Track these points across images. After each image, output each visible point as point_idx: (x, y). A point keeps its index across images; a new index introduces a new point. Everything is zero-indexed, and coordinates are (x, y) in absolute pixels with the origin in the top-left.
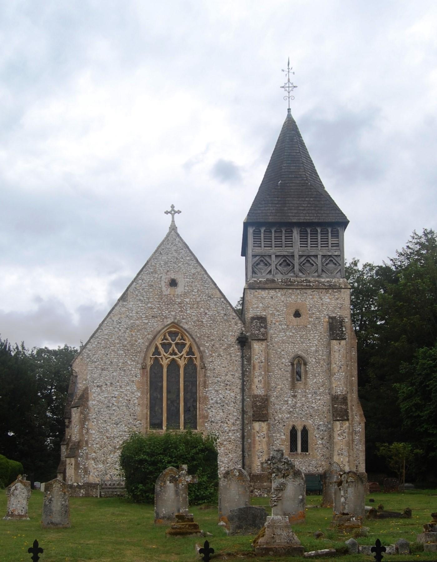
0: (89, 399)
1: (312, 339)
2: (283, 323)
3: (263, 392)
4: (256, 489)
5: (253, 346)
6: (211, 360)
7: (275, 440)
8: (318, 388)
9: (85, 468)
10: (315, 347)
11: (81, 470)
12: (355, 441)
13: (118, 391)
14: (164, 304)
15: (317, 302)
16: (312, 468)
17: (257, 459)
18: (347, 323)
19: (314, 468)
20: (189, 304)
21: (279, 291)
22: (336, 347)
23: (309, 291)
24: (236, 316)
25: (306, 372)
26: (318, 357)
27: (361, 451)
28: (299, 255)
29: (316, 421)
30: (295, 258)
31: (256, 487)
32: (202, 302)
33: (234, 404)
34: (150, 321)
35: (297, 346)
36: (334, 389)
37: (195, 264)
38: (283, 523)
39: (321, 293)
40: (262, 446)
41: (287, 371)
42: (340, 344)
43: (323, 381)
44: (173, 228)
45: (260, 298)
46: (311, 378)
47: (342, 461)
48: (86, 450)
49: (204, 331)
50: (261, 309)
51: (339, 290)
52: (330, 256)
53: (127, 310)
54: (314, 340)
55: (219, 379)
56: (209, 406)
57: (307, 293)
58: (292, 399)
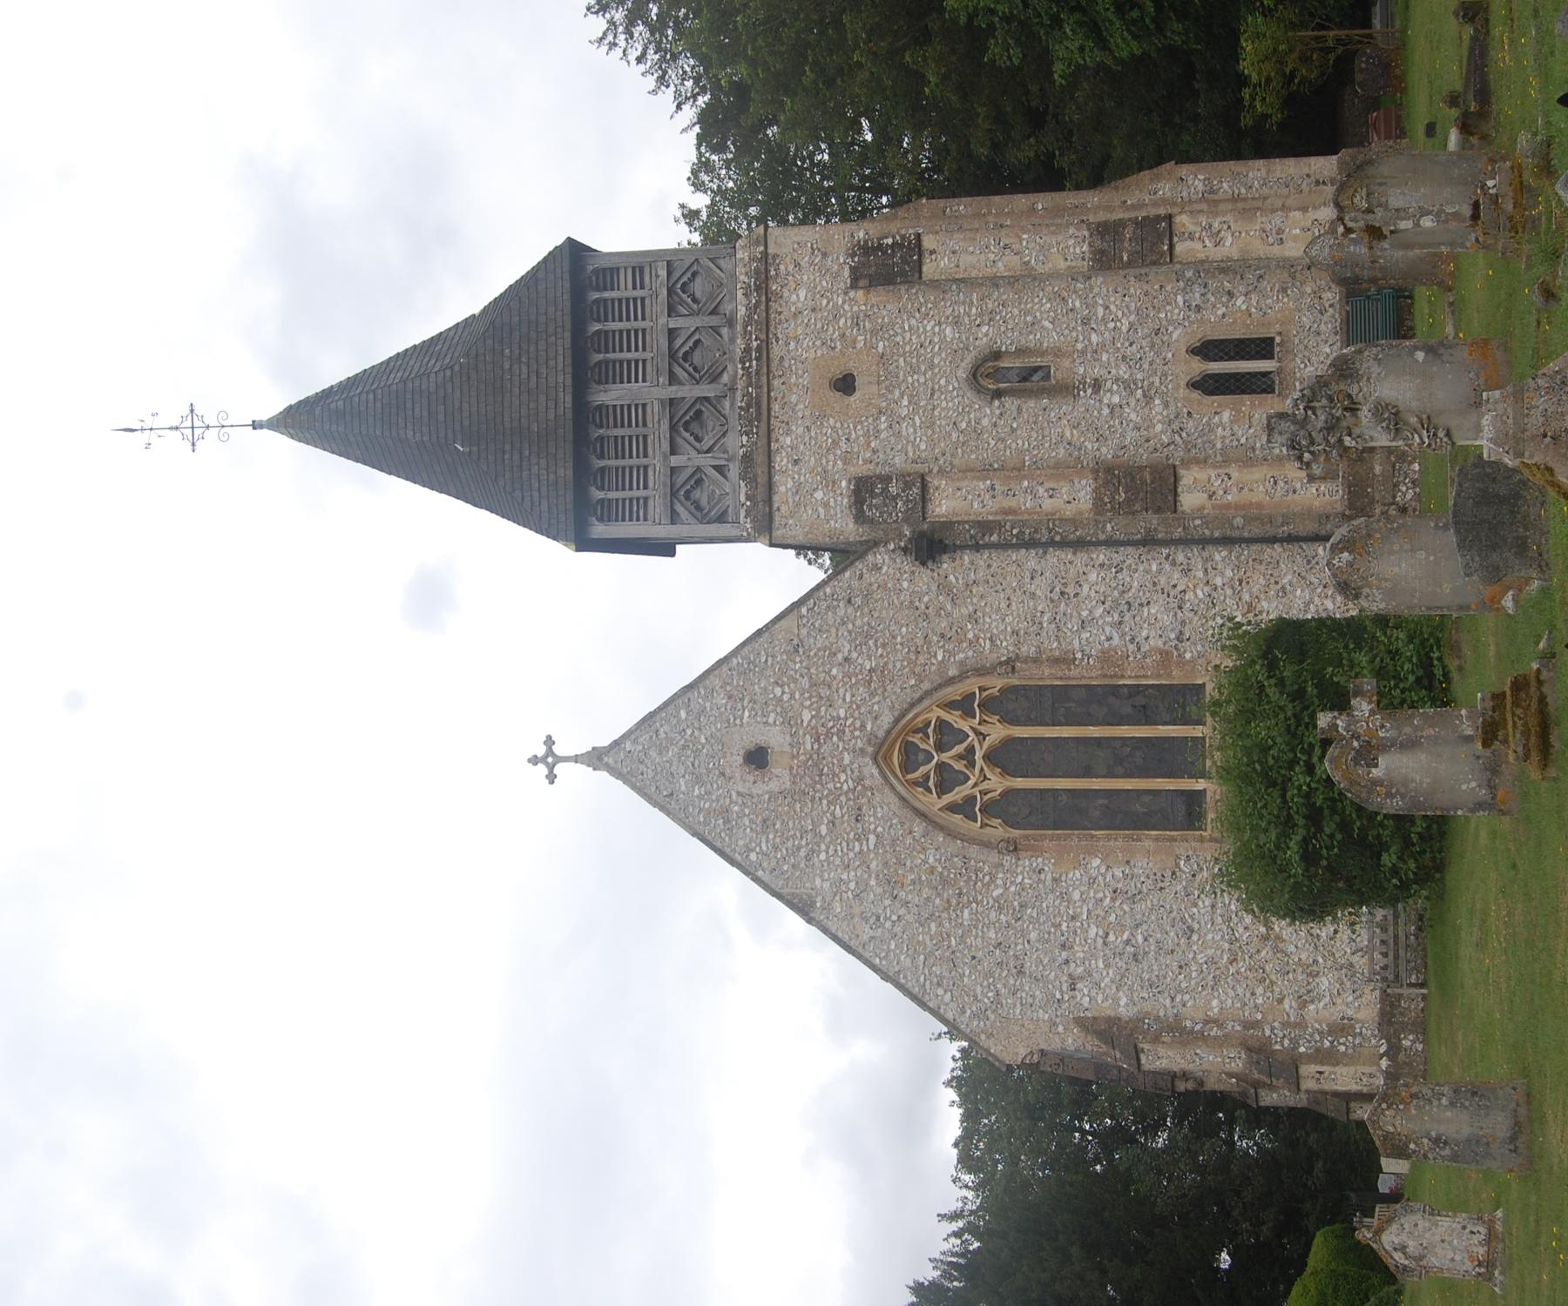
0: (1113, 1014)
1: (919, 336)
4: (1394, 497)
5: (943, 516)
7: (1235, 443)
9: (1330, 1033)
13: (1086, 925)
17: (1296, 496)
18: (871, 232)
19: (1324, 319)
21: (777, 441)
22: (945, 262)
23: (776, 351)
26: (972, 318)
29: (1175, 317)
30: (680, 395)
35: (943, 382)
36: (1073, 264)
39: (780, 313)
41: (1019, 410)
44: (595, 758)
45: (797, 499)
48: (1272, 1029)
51: (770, 261)
53: (838, 898)
56: (1131, 647)
58: (1106, 392)
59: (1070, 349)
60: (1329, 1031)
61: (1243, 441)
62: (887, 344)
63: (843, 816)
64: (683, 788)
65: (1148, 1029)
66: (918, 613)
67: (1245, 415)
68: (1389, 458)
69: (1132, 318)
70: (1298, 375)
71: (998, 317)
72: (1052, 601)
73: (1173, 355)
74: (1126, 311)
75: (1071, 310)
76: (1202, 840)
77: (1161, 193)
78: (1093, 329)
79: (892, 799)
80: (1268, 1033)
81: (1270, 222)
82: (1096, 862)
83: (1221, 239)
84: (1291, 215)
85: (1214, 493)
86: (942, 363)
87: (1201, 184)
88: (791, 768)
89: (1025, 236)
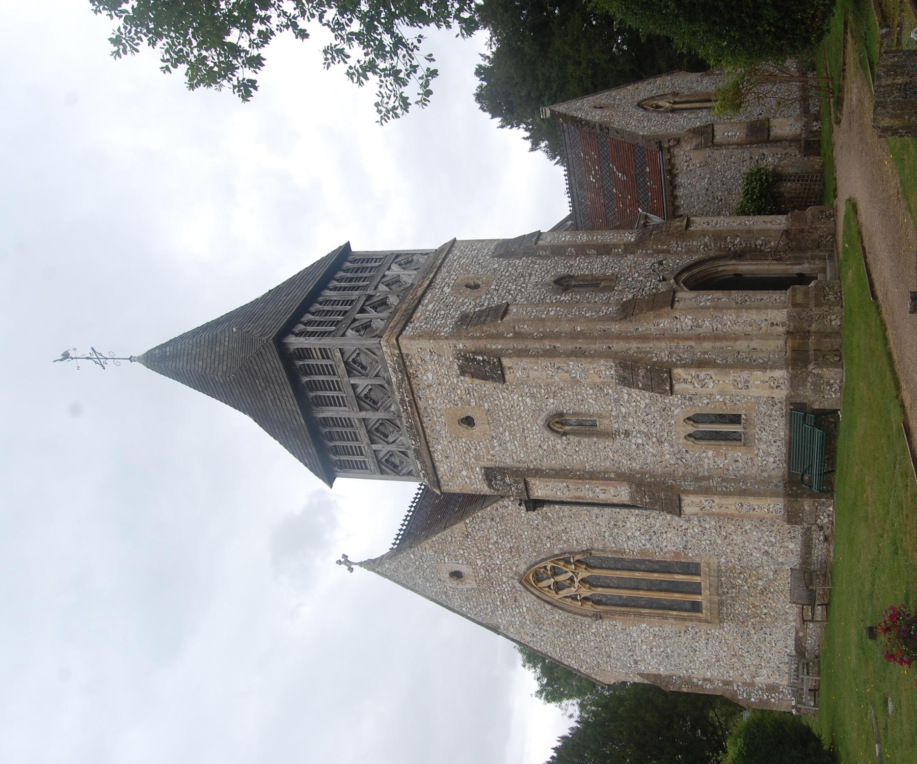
0: (657, 673)
1: (510, 402)
2: (489, 445)
3: (623, 488)
4: (816, 521)
5: (540, 497)
6: (574, 541)
7: (716, 467)
8: (606, 397)
9: (767, 690)
10: (524, 398)
11: (772, 697)
12: (715, 327)
13: (640, 645)
14: (492, 588)
15: (437, 392)
16: (776, 411)
17: (754, 512)
18: (467, 345)
19: (775, 408)
20: (485, 560)
21: (433, 447)
22: (518, 374)
23: (421, 404)
24: (491, 507)
25: (575, 414)
26: (543, 395)
27: (737, 317)
28: (360, 411)
29: (675, 403)
30: (368, 417)
31: (813, 521)
32: (478, 545)
33: (649, 518)
34: (524, 604)
35: (529, 425)
36: (606, 380)
37: (418, 549)
38: (828, 83)
39: (419, 385)
40: (730, 505)
41: (579, 442)
42: (509, 368)
43: (592, 388)
44: (371, 565)
45: (452, 474)
46: (586, 407)
47: (763, 382)
48: (738, 686)
49: (526, 547)
50: (472, 473)
51: (405, 357)
52: (346, 363)
53: (511, 626)
54: (510, 399)
55: (607, 534)
56: (657, 550)
57: (425, 408)
58: (633, 437)
59: (608, 415)
60: (766, 689)
61: (721, 466)
62: (490, 405)
63: (507, 599)
64: (421, 583)
65: (675, 683)
66: (533, 527)
67: (722, 454)
68: (814, 504)
69: (647, 401)
70: (757, 437)
71: (559, 395)
72: (610, 528)
73: (675, 422)
74: (642, 397)
75: (606, 395)
76: (700, 620)
77: (662, 325)
78: (622, 405)
79: (533, 597)
80: (735, 688)
81: (740, 376)
82: (644, 625)
83: (706, 383)
84: (754, 373)
85: (704, 508)
86: (527, 416)
87: (690, 321)
88: (476, 581)
89: (570, 363)
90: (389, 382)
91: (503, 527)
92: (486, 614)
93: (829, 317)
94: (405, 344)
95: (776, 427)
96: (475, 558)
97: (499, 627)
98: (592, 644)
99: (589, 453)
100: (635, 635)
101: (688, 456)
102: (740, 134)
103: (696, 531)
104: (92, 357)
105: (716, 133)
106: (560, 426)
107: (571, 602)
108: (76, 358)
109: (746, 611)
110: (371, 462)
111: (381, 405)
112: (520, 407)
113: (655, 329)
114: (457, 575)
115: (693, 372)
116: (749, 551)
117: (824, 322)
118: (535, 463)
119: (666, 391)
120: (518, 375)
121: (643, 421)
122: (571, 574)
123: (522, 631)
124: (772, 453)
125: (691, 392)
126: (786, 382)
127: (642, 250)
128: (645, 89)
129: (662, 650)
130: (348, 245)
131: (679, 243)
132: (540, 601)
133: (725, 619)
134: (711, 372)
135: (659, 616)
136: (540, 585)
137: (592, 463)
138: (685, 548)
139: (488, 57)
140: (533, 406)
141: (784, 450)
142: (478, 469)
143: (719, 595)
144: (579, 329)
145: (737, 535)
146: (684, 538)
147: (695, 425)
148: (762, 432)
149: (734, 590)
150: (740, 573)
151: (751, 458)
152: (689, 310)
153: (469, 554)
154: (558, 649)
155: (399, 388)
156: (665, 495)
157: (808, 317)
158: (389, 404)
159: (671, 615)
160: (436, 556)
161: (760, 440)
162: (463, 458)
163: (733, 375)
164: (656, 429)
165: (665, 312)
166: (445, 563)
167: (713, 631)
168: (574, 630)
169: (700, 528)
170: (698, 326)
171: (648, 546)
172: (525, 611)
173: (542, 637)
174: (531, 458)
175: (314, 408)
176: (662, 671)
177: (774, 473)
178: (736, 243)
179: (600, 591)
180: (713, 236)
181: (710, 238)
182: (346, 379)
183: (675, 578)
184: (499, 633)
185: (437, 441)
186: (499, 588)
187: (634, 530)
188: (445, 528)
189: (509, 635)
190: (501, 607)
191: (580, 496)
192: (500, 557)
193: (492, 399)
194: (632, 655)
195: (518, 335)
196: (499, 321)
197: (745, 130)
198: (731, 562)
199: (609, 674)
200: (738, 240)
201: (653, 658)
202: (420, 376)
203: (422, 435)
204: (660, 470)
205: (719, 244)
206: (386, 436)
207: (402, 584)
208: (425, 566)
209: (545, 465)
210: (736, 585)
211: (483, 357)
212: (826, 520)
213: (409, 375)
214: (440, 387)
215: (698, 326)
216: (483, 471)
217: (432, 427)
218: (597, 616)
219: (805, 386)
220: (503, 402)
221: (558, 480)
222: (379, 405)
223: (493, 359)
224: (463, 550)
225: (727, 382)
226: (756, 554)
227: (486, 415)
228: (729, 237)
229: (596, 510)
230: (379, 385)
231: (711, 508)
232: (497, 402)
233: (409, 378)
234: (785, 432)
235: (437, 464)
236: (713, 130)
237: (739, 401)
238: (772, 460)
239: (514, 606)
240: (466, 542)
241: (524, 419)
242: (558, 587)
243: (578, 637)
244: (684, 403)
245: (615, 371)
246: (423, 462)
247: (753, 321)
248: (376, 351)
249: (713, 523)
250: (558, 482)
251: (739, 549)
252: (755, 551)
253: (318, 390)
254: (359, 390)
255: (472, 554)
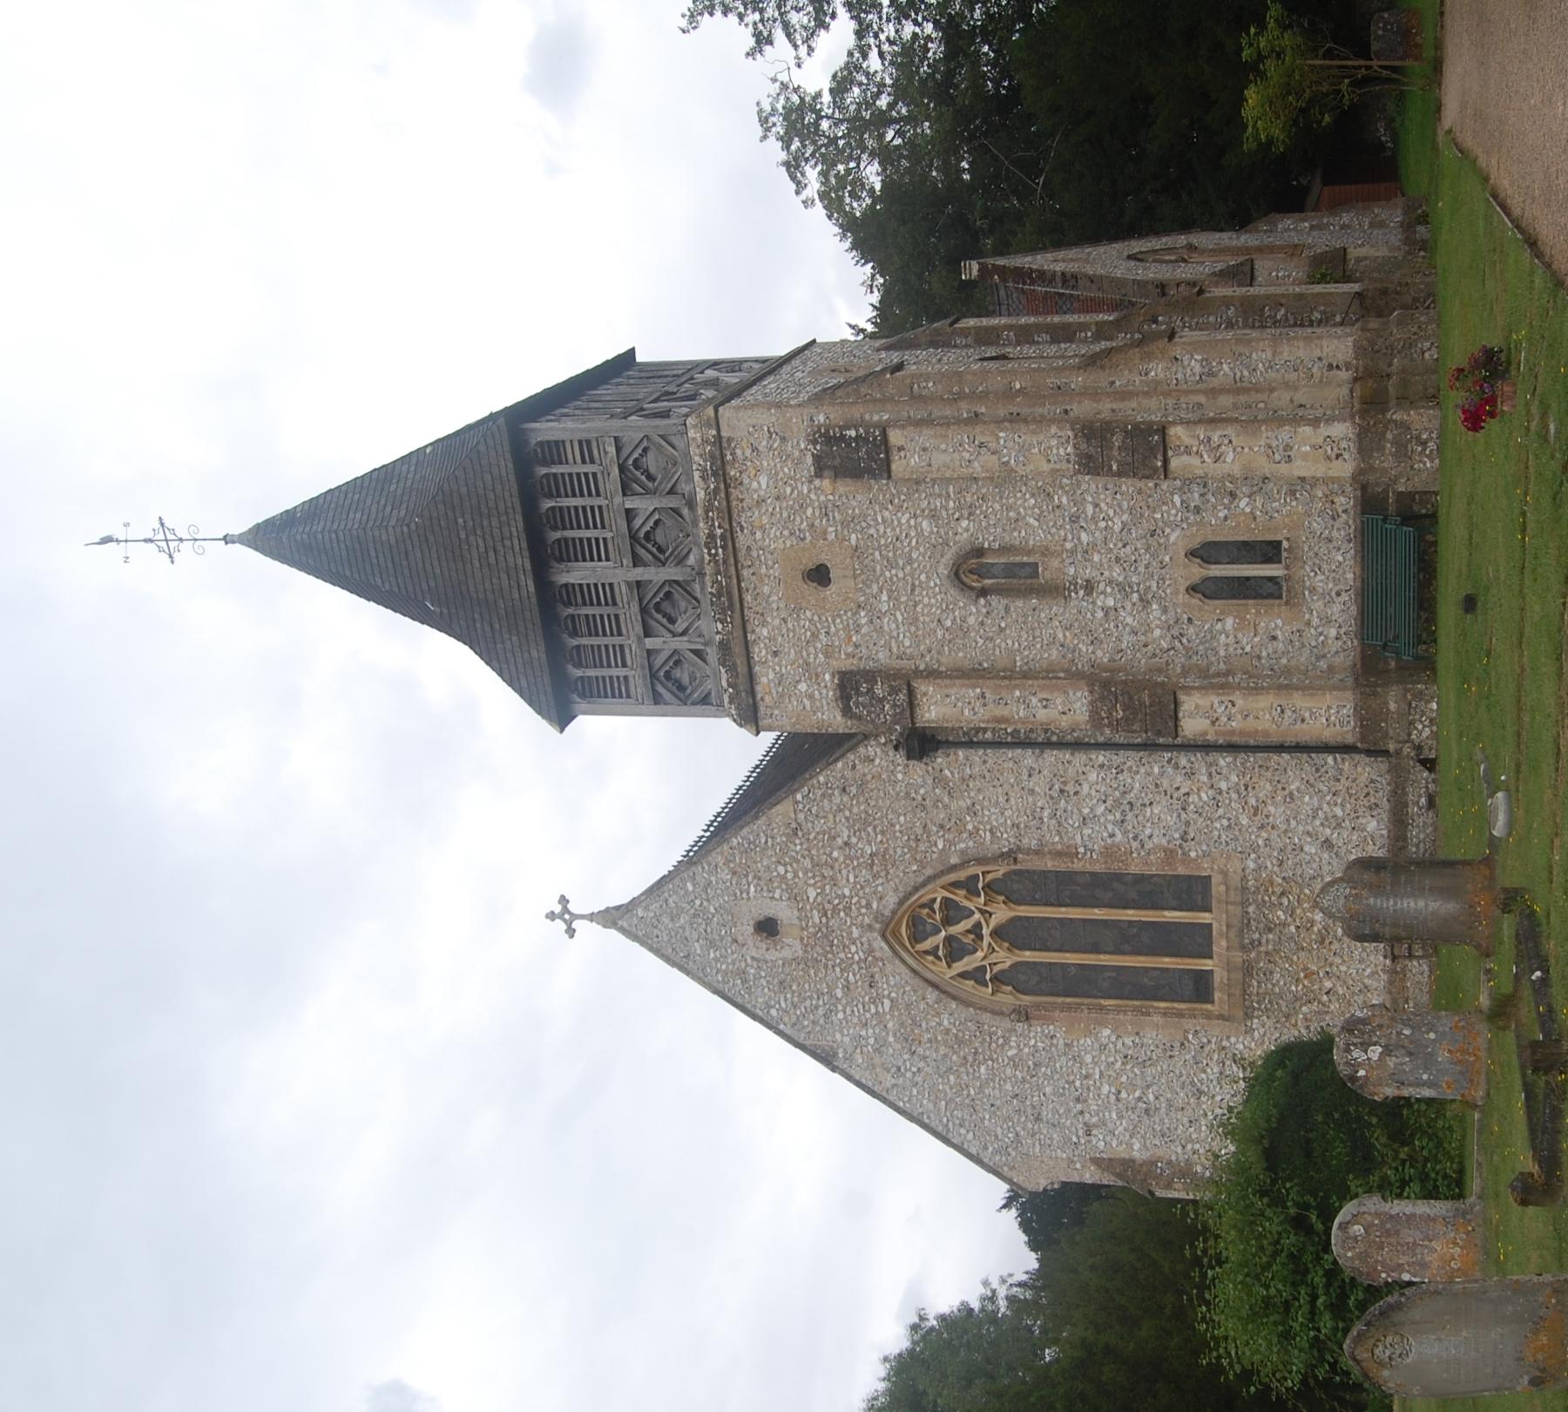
0: (1127, 1157)
1: (893, 529)
2: (851, 621)
3: (1079, 694)
4: (1409, 735)
5: (933, 721)
6: (988, 833)
7: (1240, 651)
8: (1057, 513)
10: (920, 519)
13: (1098, 1084)
14: (830, 956)
15: (772, 514)
16: (1338, 529)
17: (1304, 726)
18: (832, 416)
19: (1337, 525)
21: (753, 631)
23: (742, 540)
24: (845, 760)
27: (1274, 355)
28: (635, 566)
29: (1172, 519)
30: (646, 577)
33: (1122, 771)
34: (886, 993)
35: (923, 577)
36: (1058, 467)
37: (703, 868)
39: (742, 501)
41: (1007, 609)
42: (901, 449)
44: (611, 918)
45: (780, 689)
46: (1023, 533)
47: (1313, 447)
49: (899, 851)
52: (622, 469)
53: (858, 1051)
54: (896, 522)
56: (1135, 845)
61: (1248, 649)
62: (859, 536)
63: (856, 982)
64: (699, 951)
65: (1161, 1174)
66: (915, 804)
67: (1249, 624)
68: (1405, 696)
69: (1125, 517)
70: (1308, 584)
71: (978, 512)
72: (1052, 798)
73: (1171, 559)
74: (1118, 510)
75: (1058, 507)
76: (1209, 1016)
77: (1153, 373)
78: (1082, 527)
79: (903, 968)
81: (1276, 437)
82: (1106, 1032)
84: (1300, 430)
85: (1217, 719)
86: (921, 558)
87: (1198, 365)
88: (802, 939)
89: (1002, 434)
90: (691, 503)
91: (862, 807)
92: (813, 1022)
93: (1420, 345)
94: (729, 419)
95: (1340, 563)
96: (806, 882)
97: (835, 1055)
98: (1008, 1087)
99: (1023, 633)
100: (1088, 1059)
101: (1192, 630)
102: (1298, 273)
103: (1205, 798)
104: (156, 538)
105: (1257, 273)
106: (975, 577)
107: (973, 986)
108: (126, 541)
109: (1293, 988)
110: (638, 683)
111: (672, 552)
112: (910, 541)
113: (1141, 381)
114: (768, 928)
115: (1201, 432)
116: (1297, 840)
117: (1411, 354)
118: (928, 659)
119: (1156, 470)
120: (913, 463)
121: (1118, 560)
122: (977, 916)
123: (877, 1061)
124: (1333, 618)
125: (1196, 471)
126: (1352, 445)
127: (1126, 334)
128: (1137, 246)
129: (1137, 1094)
130: (632, 352)
131: (1187, 319)
132: (918, 981)
133: (1254, 1009)
134: (1230, 431)
135: (1135, 1010)
136: (920, 947)
137: (1026, 653)
138: (1184, 838)
139: (863, 331)
140: (933, 536)
141: (1354, 610)
142: (827, 677)
143: (1243, 948)
144: (1018, 386)
145: (1275, 804)
146: (1183, 815)
147: (1205, 565)
148: (1316, 573)
149: (1271, 936)
150: (1283, 894)
151: (1298, 631)
152: (1195, 347)
153: (796, 875)
154: (943, 1103)
155: (707, 512)
156: (1150, 697)
157: (1387, 348)
158: (686, 550)
159: (1156, 1008)
160: (734, 882)
161: (1313, 590)
162: (804, 654)
163: (1266, 435)
164: (1139, 574)
165: (1158, 348)
166: (749, 899)
167: (1233, 1040)
168: (975, 1053)
169: (1211, 792)
170: (1212, 374)
171: (1119, 837)
172: (887, 1010)
173: (914, 1073)
174: (922, 648)
175: (555, 564)
176: (1138, 1152)
177: (1338, 660)
178: (1279, 317)
179: (1029, 957)
180: (1242, 305)
181: (1236, 308)
182: (618, 499)
183: (1164, 917)
184: (834, 1069)
185: (761, 618)
186: (842, 955)
187: (1095, 801)
188: (757, 817)
189: (853, 1072)
190: (844, 1001)
191: (1002, 717)
192: (852, 880)
193: (864, 524)
194: (1082, 1112)
195: (916, 398)
196: (888, 376)
197: (1306, 268)
198: (1266, 867)
199: (1037, 1164)
200: (1282, 312)
201: (1120, 1117)
202: (746, 481)
203: (737, 606)
204: (1143, 662)
205: (1251, 320)
206: (672, 621)
207: (667, 959)
208: (712, 910)
209: (946, 660)
210: (1275, 925)
211: (857, 431)
212: (1427, 732)
213: (729, 481)
214: (778, 504)
215: (1212, 374)
216: (836, 681)
217: (755, 588)
218: (1020, 1012)
219: (1381, 449)
220: (882, 531)
221: (967, 682)
222: (667, 554)
223: (874, 431)
224: (785, 865)
225: (1256, 449)
226: (1310, 849)
227: (852, 558)
228: (1267, 308)
229: (1028, 758)
230: (671, 509)
231: (1229, 719)
232: (872, 531)
233: (727, 487)
234: (1354, 574)
235: (757, 669)
236: (1252, 269)
237: (1278, 512)
238: (1333, 632)
239: (867, 999)
240: (792, 847)
241: (916, 565)
242: (955, 951)
243: (983, 1069)
244: (1187, 519)
245: (1074, 445)
246: (732, 669)
247: (1299, 361)
248: (674, 440)
249: (1234, 778)
250: (967, 686)
251: (1279, 836)
252: (1309, 839)
253: (564, 528)
254: (638, 522)
255: (801, 875)
